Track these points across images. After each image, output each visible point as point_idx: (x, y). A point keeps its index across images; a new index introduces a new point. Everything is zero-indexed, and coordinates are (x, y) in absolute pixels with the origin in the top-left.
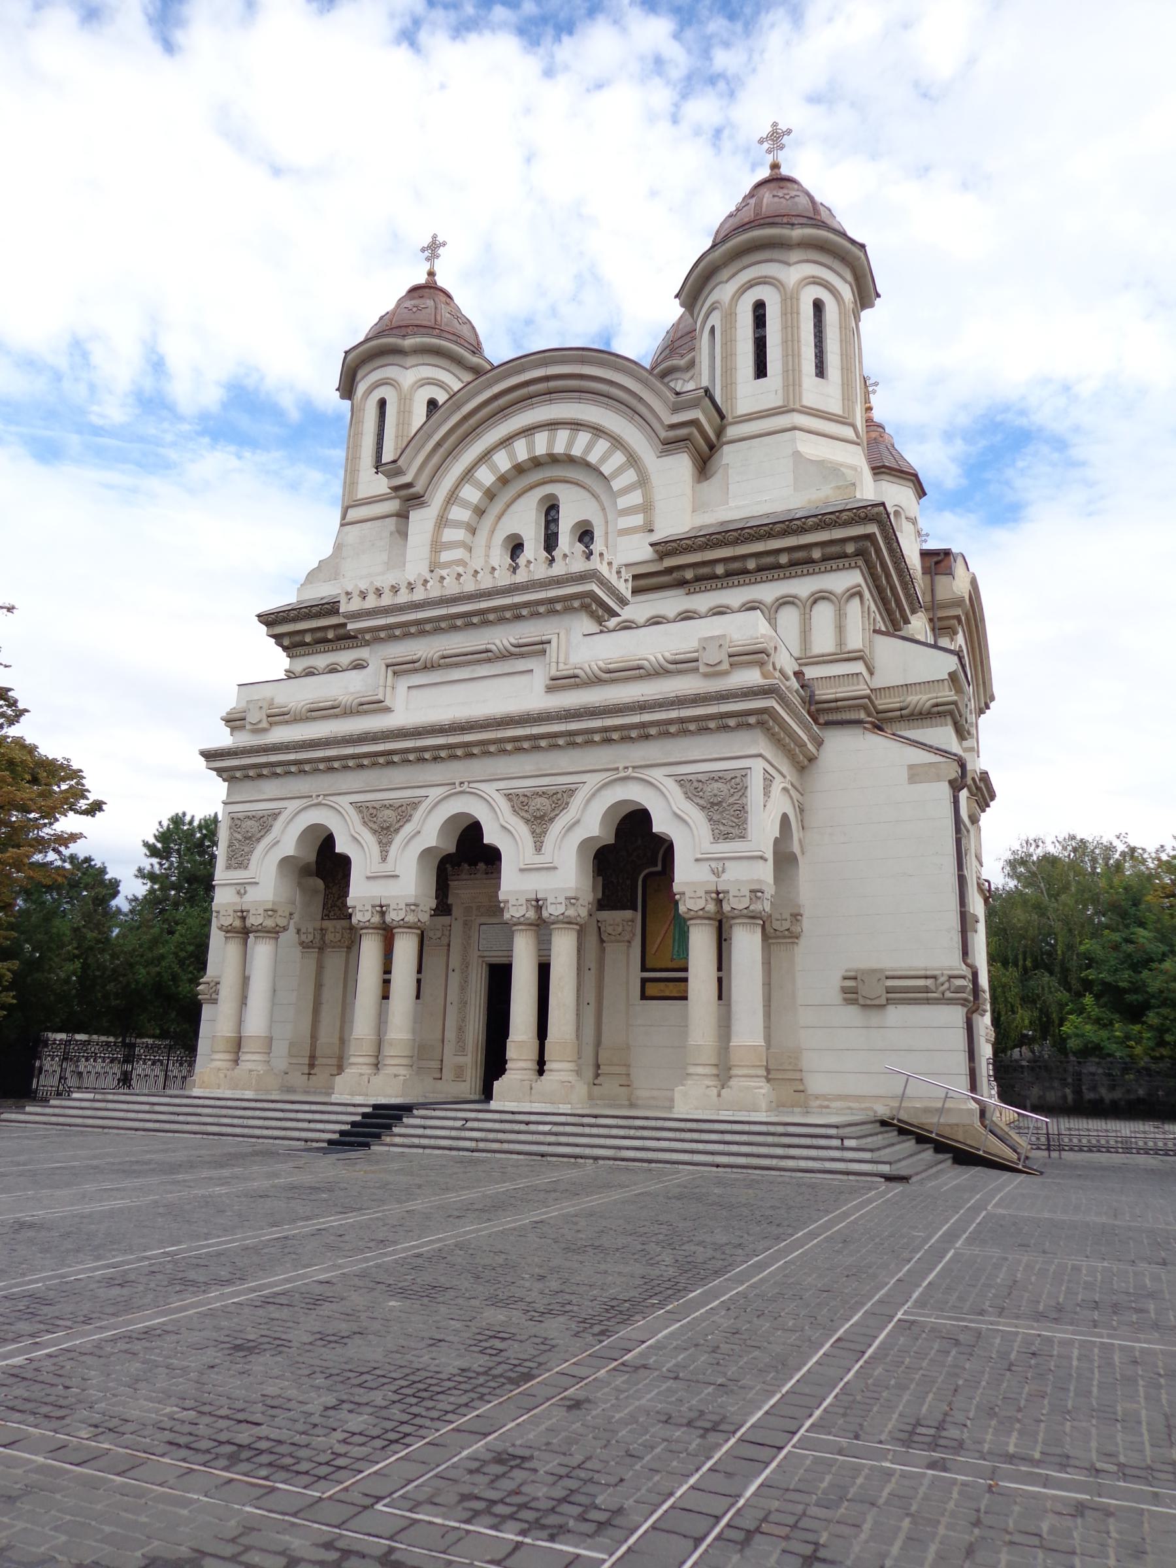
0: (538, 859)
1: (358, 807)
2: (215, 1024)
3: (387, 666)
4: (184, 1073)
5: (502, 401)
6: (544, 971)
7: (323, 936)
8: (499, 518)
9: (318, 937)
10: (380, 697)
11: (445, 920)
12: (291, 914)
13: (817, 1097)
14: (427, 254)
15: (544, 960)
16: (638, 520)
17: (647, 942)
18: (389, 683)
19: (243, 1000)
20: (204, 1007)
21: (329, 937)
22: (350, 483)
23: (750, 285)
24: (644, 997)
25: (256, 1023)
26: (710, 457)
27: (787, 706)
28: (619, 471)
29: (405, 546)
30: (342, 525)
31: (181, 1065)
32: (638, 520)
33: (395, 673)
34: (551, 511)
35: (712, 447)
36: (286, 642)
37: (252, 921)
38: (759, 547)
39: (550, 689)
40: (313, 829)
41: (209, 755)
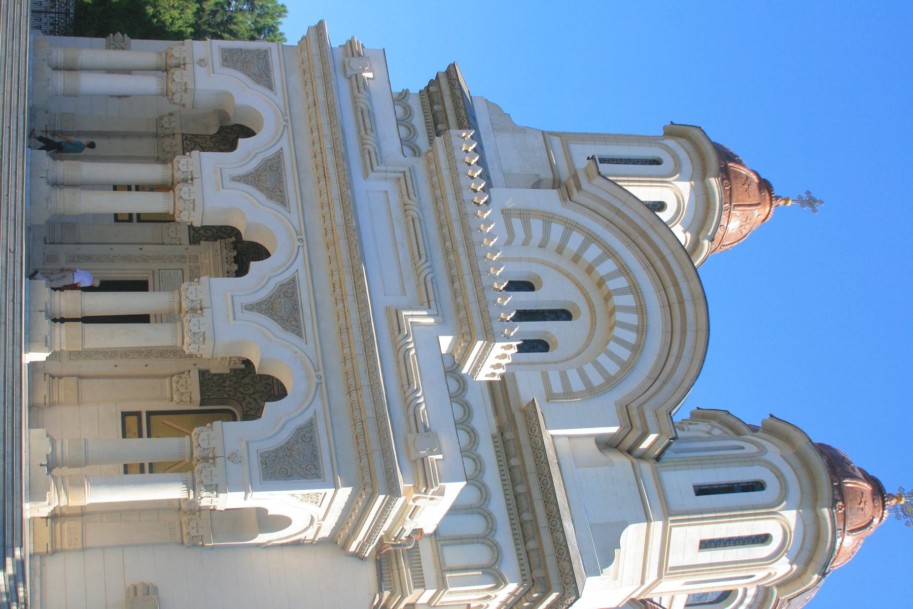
0: (238, 308)
1: (279, 155)
2: (91, 50)
4: (44, 27)
5: (659, 264)
6: (144, 319)
7: (166, 136)
8: (557, 268)
9: (168, 132)
10: (376, 168)
11: (185, 237)
12: (184, 105)
13: (42, 565)
14: (805, 196)
15: (152, 318)
16: (557, 387)
17: (179, 416)
18: (389, 175)
19: (111, 71)
20: (104, 39)
21: (168, 141)
23: (780, 476)
24: (125, 415)
25: (91, 83)
26: (621, 451)
29: (527, 188)
30: (543, 132)
31: (51, 24)
32: (557, 387)
33: (399, 179)
34: (563, 315)
35: (629, 452)
36: (432, 89)
37: (177, 74)
38: (536, 494)
39: (388, 309)
40: (259, 119)
41: (319, 28)
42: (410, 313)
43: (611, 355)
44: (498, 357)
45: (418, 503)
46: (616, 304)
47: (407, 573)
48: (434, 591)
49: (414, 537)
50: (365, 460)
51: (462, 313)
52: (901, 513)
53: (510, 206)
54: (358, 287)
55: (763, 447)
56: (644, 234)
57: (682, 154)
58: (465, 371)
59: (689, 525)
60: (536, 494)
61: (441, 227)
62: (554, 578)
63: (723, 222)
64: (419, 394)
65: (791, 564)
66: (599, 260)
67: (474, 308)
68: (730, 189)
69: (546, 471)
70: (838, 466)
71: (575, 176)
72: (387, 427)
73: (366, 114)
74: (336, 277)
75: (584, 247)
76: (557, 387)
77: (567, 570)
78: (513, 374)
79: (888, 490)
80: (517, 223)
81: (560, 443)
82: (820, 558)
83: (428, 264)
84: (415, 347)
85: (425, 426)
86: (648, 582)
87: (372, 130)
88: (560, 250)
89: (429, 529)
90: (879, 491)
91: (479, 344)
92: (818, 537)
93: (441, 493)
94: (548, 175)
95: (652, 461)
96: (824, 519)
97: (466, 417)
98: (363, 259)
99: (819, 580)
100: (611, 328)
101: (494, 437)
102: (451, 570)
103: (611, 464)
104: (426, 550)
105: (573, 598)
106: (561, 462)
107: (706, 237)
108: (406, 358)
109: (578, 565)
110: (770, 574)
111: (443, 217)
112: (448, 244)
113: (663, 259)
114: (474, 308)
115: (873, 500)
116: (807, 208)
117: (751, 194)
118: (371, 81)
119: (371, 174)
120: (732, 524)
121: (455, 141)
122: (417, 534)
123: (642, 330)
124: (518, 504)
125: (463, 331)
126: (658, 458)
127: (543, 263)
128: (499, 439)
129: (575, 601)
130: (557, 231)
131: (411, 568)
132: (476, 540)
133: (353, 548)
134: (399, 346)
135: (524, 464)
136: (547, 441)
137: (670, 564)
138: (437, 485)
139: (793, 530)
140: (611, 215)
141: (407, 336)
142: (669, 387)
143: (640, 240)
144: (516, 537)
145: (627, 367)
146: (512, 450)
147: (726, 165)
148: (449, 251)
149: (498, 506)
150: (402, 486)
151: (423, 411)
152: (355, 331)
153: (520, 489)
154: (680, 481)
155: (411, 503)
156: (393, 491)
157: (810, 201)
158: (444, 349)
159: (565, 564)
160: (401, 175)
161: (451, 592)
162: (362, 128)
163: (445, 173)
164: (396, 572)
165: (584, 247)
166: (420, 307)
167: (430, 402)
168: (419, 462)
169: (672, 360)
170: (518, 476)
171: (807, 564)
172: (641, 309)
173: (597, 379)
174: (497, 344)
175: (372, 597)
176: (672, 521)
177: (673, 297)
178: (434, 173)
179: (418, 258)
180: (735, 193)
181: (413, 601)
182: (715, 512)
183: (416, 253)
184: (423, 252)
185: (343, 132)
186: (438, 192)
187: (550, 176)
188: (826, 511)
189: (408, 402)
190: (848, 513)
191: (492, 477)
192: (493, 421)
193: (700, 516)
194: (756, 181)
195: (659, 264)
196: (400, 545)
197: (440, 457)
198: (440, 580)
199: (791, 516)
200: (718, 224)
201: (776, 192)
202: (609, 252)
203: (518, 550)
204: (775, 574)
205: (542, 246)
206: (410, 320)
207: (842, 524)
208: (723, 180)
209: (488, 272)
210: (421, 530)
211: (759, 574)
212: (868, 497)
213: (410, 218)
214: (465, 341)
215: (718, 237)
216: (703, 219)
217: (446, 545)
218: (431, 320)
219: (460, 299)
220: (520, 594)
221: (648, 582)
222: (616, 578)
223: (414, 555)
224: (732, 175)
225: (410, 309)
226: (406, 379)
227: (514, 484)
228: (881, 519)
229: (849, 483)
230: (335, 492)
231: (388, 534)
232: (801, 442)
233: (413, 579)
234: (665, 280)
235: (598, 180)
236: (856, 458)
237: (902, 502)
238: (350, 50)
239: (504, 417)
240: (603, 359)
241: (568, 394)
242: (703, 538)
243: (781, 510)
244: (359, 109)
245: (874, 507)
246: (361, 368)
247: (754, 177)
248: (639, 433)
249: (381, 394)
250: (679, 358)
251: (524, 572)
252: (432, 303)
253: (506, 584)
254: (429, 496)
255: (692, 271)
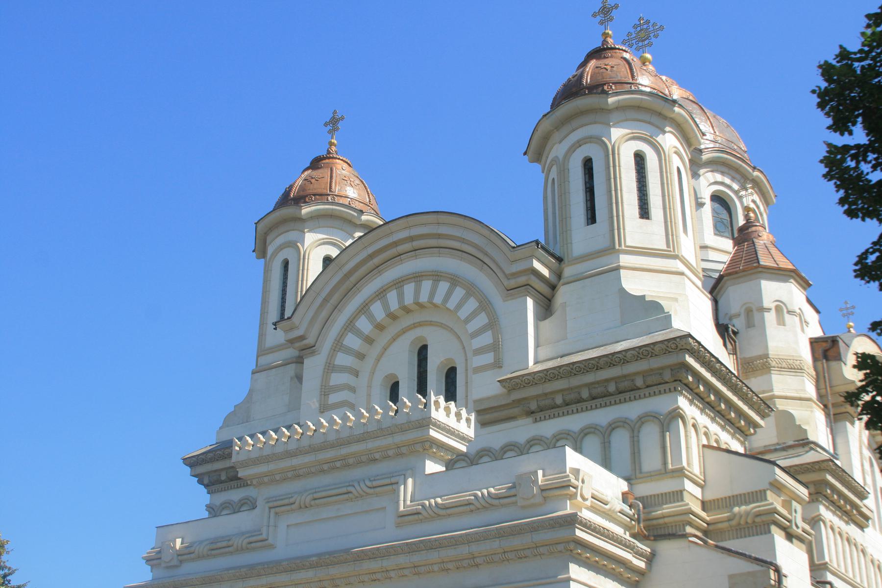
3: (270, 508)
5: (376, 261)
10: (264, 536)
18: (272, 523)
22: (262, 336)
23: (579, 144)
26: (553, 296)
27: (598, 532)
28: (473, 315)
33: (276, 513)
34: (422, 353)
35: (553, 287)
36: (206, 481)
38: (590, 378)
42: (402, 503)
43: (459, 306)
44: (448, 415)
45: (588, 495)
46: (412, 301)
47: (667, 509)
48: (686, 481)
49: (631, 500)
50: (541, 550)
51: (404, 450)
52: (646, 42)
53: (317, 405)
54: (374, 555)
55: (552, 160)
56: (348, 276)
57: (280, 240)
58: (464, 449)
59: (624, 229)
60: (590, 378)
61: (322, 471)
62: (671, 360)
63: (346, 201)
64: (479, 494)
65: (664, 132)
66: (371, 317)
67: (398, 438)
68: (314, 195)
69: (568, 368)
70: (572, 90)
71: (291, 342)
72: (509, 527)
73: (214, 546)
74: (366, 578)
75: (358, 333)
76: (489, 358)
77: (664, 347)
78: (475, 402)
79: (599, 44)
80: (333, 398)
81: (543, 355)
82: (659, 105)
83: (356, 485)
84: (434, 498)
85: (510, 488)
86: (681, 267)
87: (229, 540)
88: (361, 356)
89: (624, 486)
90: (598, 53)
91: (433, 433)
92: (637, 108)
93: (576, 472)
94: (291, 369)
95: (563, 265)
96: (619, 101)
97: (516, 449)
98: (347, 551)
99: (681, 106)
100: (435, 306)
101: (536, 421)
102: (665, 463)
103: (564, 305)
104: (646, 489)
105: (691, 340)
106: (561, 353)
107: (359, 218)
108: (445, 507)
109: (659, 336)
110: (676, 153)
111: (313, 470)
112: (338, 464)
113: (371, 257)
114: (398, 438)
115: (605, 58)
116: (340, 125)
117: (321, 176)
118: (185, 540)
119: (270, 541)
120: (624, 189)
121: (242, 457)
122: (627, 498)
123: (437, 276)
124: (600, 396)
125: (421, 450)
126: (560, 260)
127: (373, 373)
128: (538, 416)
129: (693, 338)
130: (342, 359)
131: (663, 504)
132: (636, 439)
133: (642, 564)
134: (433, 515)
135: (562, 390)
136: (539, 367)
137: (665, 247)
138: (568, 476)
139: (629, 131)
140: (329, 306)
141: (423, 506)
142: (489, 249)
143: (353, 279)
144: (632, 398)
145: (472, 290)
146: (547, 402)
147: (292, 199)
148: (346, 464)
149: (602, 416)
150: (569, 511)
151: (496, 490)
152: (416, 558)
153: (585, 394)
154: (582, 238)
155: (588, 503)
156: (572, 521)
157: (334, 123)
158: (439, 468)
159: (657, 348)
160: (273, 511)
161: (688, 464)
162: (227, 550)
163: (272, 467)
164: (666, 520)
165: (358, 333)
166: (396, 493)
167: (488, 484)
168: (545, 494)
169: (465, 247)
170: (573, 396)
171: (665, 118)
172: (417, 277)
173: (482, 320)
174: (433, 415)
175: (691, 544)
176: (620, 245)
177: (407, 247)
178: (272, 479)
179: (350, 495)
180: (319, 191)
181: (699, 503)
182: (611, 204)
183: (346, 496)
184: (344, 490)
185: (228, 569)
186: (290, 475)
187: (293, 365)
188: (611, 100)
189: (487, 505)
190: (615, 80)
191: (575, 422)
192: (521, 422)
193: (615, 218)
194: (310, 171)
195: (376, 261)
196: (639, 515)
197: (540, 473)
198: (675, 474)
199: (616, 133)
200: (348, 207)
201: (324, 153)
202: (364, 309)
203: (645, 397)
204: (676, 147)
205: (356, 374)
206: (408, 503)
207: (628, 85)
208: (305, 202)
209: (364, 424)
210: (623, 494)
211: (676, 162)
212: (601, 63)
213: (313, 503)
214: (431, 447)
215: (359, 206)
216: (338, 220)
217: (640, 469)
218: (410, 481)
219: (390, 453)
220: (690, 394)
221: (681, 267)
222: (676, 300)
223: (648, 502)
224: (302, 193)
225: (398, 502)
226: (465, 508)
227: (580, 400)
228: (625, 51)
229: (587, 79)
230: (574, 581)
231: (627, 528)
232: (547, 125)
233: (674, 502)
234: (392, 254)
235: (295, 319)
236: (570, 72)
237: (610, 32)
238: (155, 562)
239: (515, 411)
240: (463, 313)
241: (495, 347)
242: (638, 215)
243: (610, 141)
244: (209, 552)
245: (612, 57)
246: (450, 553)
247: (306, 173)
248: (533, 277)
249: (476, 533)
250: (463, 240)
251: (667, 390)
252: (393, 480)
253: (678, 408)
254: (580, 484)
255: (387, 227)
